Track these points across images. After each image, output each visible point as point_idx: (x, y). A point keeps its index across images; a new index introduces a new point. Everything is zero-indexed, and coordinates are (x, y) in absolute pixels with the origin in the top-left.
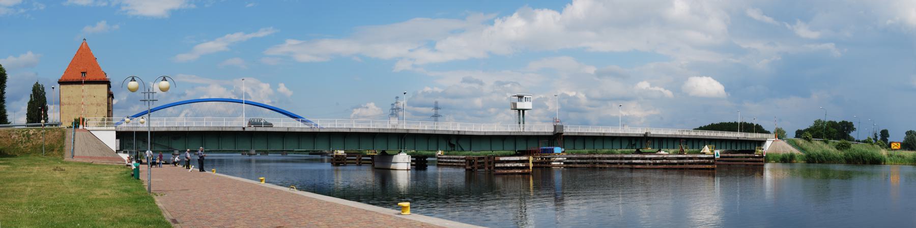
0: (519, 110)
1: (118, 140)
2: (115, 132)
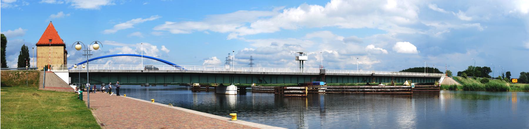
0: (300, 61)
1: (70, 78)
2: (68, 73)
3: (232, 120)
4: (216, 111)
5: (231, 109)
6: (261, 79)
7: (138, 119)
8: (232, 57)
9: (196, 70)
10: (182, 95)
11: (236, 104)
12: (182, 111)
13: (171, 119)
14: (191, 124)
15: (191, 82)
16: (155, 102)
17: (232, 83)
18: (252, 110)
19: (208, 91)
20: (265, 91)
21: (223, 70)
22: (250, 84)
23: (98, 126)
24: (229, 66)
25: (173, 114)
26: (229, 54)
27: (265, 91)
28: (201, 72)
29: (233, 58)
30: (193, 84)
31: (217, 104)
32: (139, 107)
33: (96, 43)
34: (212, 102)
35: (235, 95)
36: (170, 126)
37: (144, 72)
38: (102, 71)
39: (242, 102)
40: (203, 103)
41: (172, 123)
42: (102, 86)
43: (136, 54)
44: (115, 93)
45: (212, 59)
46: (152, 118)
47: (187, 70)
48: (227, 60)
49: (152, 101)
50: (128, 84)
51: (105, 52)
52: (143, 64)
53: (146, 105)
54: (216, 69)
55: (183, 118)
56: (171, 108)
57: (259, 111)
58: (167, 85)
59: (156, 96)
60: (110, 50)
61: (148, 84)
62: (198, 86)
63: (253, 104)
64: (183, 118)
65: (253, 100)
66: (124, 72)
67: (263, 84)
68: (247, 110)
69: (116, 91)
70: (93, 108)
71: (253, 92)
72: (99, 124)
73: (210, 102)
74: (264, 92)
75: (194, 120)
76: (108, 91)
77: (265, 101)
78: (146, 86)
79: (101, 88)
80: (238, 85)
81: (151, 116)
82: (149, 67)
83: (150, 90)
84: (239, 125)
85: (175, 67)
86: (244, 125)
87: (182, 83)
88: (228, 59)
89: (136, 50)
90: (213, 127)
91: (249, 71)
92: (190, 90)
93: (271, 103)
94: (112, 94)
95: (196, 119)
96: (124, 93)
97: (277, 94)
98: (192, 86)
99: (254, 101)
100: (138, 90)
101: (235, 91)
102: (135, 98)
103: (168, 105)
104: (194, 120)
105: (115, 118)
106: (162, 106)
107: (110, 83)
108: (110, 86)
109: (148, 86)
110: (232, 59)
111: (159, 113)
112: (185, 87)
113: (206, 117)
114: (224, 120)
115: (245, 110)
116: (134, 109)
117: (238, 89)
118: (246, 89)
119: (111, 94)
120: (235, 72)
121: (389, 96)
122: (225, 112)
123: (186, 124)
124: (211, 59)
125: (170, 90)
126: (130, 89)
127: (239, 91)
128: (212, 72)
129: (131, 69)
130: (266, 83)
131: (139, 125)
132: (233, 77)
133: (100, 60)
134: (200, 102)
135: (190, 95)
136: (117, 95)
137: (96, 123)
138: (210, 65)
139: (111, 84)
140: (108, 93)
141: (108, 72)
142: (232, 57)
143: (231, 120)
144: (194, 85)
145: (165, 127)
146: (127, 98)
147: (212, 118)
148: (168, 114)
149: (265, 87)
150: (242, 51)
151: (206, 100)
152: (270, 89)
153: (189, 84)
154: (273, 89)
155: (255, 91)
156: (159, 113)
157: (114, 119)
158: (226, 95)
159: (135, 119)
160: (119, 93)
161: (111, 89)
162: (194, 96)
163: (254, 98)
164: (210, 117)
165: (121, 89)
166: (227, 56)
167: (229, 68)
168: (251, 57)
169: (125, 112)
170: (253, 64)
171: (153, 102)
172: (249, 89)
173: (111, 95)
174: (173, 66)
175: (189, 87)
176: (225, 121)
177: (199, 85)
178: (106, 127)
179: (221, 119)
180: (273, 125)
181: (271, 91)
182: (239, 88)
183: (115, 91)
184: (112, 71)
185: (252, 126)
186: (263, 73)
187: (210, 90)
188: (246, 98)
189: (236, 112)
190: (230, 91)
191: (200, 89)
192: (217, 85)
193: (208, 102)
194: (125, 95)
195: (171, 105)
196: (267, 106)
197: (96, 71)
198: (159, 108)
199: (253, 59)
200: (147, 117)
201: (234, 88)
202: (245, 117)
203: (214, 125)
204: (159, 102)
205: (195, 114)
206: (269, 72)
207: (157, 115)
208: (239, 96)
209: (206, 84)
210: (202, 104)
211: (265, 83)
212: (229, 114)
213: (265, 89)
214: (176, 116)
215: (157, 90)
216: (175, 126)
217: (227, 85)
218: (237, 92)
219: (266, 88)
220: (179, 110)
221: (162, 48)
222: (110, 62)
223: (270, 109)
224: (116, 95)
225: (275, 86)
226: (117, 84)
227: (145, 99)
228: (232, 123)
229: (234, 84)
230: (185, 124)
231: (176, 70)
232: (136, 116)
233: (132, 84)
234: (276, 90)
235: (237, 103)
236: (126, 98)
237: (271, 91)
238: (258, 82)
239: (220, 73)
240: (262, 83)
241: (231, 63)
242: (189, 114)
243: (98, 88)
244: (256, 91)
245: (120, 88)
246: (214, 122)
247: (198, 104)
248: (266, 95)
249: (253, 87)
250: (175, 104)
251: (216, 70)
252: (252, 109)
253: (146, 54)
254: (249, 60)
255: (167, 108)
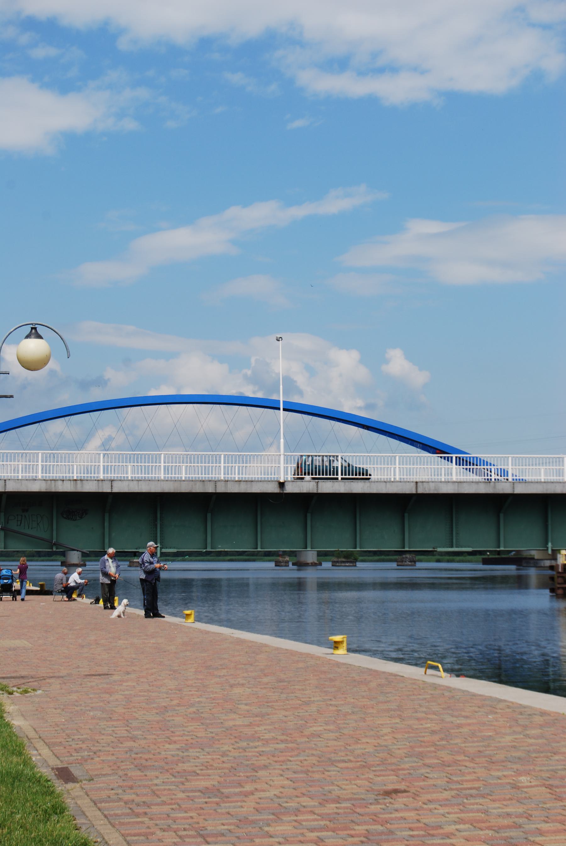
7: (260, 743)
10: (499, 614)
12: (266, 646)
13: (434, 745)
14: (555, 771)
15: (547, 543)
16: (349, 650)
23: (38, 780)
25: (449, 719)
32: (265, 680)
33: (34, 333)
36: (431, 782)
37: (290, 489)
38: (68, 488)
41: (444, 764)
42: (65, 569)
43: (249, 392)
44: (140, 603)
46: (332, 735)
49: (336, 645)
50: (208, 553)
51: (84, 385)
52: (287, 447)
53: (301, 665)
55: (509, 738)
56: (435, 687)
58: (414, 562)
59: (359, 619)
60: (109, 374)
61: (311, 556)
64: (509, 738)
66: (184, 488)
69: (140, 591)
70: (15, 682)
72: (45, 772)
76: (100, 592)
78: (301, 565)
79: (59, 575)
81: (332, 727)
82: (318, 462)
83: (323, 586)
85: (460, 461)
87: (499, 553)
89: (249, 372)
92: (542, 586)
94: (120, 609)
96: (187, 602)
98: (552, 568)
100: (259, 586)
102: (241, 628)
103: (421, 670)
105: (134, 739)
106: (391, 674)
107: (111, 550)
108: (112, 568)
109: (314, 564)
111: (371, 711)
112: (511, 569)
116: (237, 690)
119: (113, 608)
123: (528, 773)
125: (433, 585)
126: (219, 580)
129: (222, 477)
131: (261, 773)
133: (57, 425)
135: (541, 612)
136: (147, 616)
137: (26, 762)
139: (112, 556)
140: (97, 601)
141: (100, 491)
145: (402, 787)
146: (201, 631)
148: (420, 715)
156: (371, 711)
157: (130, 744)
159: (244, 744)
160: (159, 604)
161: (113, 582)
165: (169, 583)
169: (192, 705)
171: (342, 651)
173: (116, 613)
174: (450, 460)
175: (532, 572)
178: (88, 786)
183: (138, 593)
184: (118, 488)
185: (274, 645)
194: (188, 616)
195: (436, 668)
197: (35, 487)
198: (373, 685)
200: (307, 732)
204: (373, 653)
207: (364, 720)
214: (465, 730)
215: (360, 586)
216: (458, 782)
220: (483, 698)
221: (387, 361)
222: (110, 439)
224: (143, 613)
226: (147, 557)
227: (296, 637)
230: (519, 773)
231: (462, 478)
232: (250, 725)
233: (226, 553)
236: (195, 629)
242: (538, 719)
243: (42, 576)
245: (163, 575)
250: (457, 662)
253: (301, 393)
255: (414, 682)
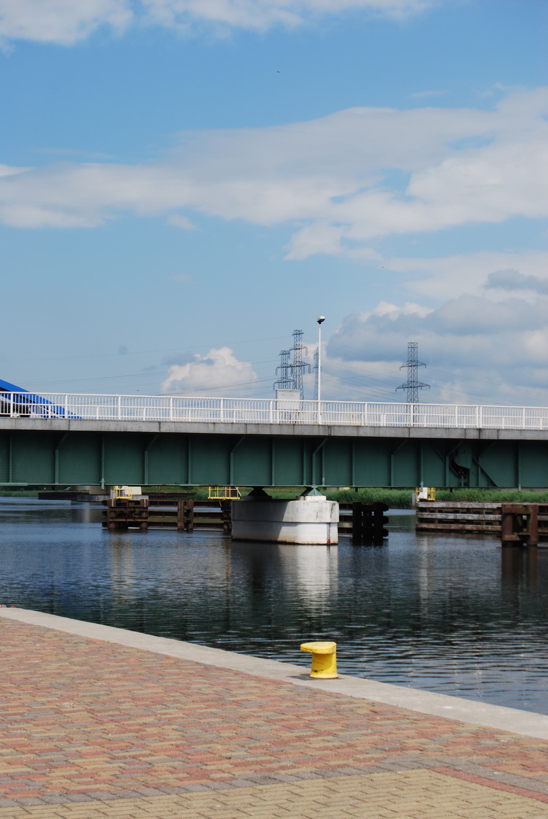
3: (314, 675)
4: (228, 627)
5: (310, 619)
6: (465, 461)
8: (312, 349)
9: (127, 417)
10: (52, 545)
11: (332, 595)
14: (97, 696)
17: (314, 486)
18: (418, 628)
19: (187, 524)
20: (453, 526)
21: (266, 415)
22: (406, 492)
24: (297, 395)
26: (298, 333)
27: (453, 526)
28: (154, 429)
29: (317, 354)
30: (108, 488)
31: (234, 592)
34: (210, 584)
35: (329, 544)
39: (364, 581)
40: (161, 590)
45: (210, 362)
47: (80, 419)
48: (285, 367)
54: (231, 414)
57: (452, 631)
62: (137, 502)
63: (424, 595)
65: (424, 573)
67: (475, 491)
68: (389, 625)
71: (420, 532)
73: (198, 582)
74: (447, 532)
75: (118, 679)
77: (451, 575)
80: (345, 495)
84: (351, 701)
86: (373, 704)
87: (54, 487)
88: (290, 362)
90: (215, 715)
91: (402, 424)
92: (94, 520)
93: (483, 588)
95: (125, 673)
97: (514, 544)
98: (105, 503)
99: (429, 578)
101: (325, 526)
104: (118, 679)
110: (312, 362)
112: (66, 504)
113: (177, 663)
114: (272, 677)
115: (381, 624)
117: (343, 518)
118: (385, 513)
120: (329, 427)
121: (453, 534)
122: (275, 634)
123: (71, 699)
124: (203, 362)
127: (347, 525)
128: (210, 430)
130: (492, 485)
132: (320, 454)
134: (144, 583)
135: (93, 545)
138: (200, 389)
142: (312, 349)
143: (305, 677)
144: (114, 496)
147: (207, 668)
149: (451, 505)
150: (364, 317)
151: (179, 573)
152: (475, 517)
153: (88, 488)
154: (491, 517)
155: (432, 526)
158: (283, 549)
162: (112, 551)
163: (425, 563)
164: (198, 663)
166: (288, 344)
167: (297, 406)
168: (413, 347)
170: (422, 385)
172: (403, 519)
175: (86, 508)
176: (278, 684)
177: (143, 494)
179: (255, 673)
180: (526, 704)
181: (484, 527)
182: (349, 513)
185: (415, 709)
186: (473, 435)
187: (196, 520)
188: (387, 561)
189: (336, 633)
190: (300, 526)
191: (144, 515)
192: (234, 493)
193: (190, 582)
196: (459, 602)
199: (421, 359)
201: (321, 511)
202: (379, 664)
203: (220, 701)
205: (121, 646)
206: (503, 426)
208: (348, 550)
209: (179, 491)
210: (155, 595)
211: (483, 482)
212: (297, 646)
213: (451, 516)
214: (13, 658)
217: (288, 495)
218: (341, 530)
219: (456, 511)
223: (477, 618)
225: (505, 500)
228: (315, 693)
229: (322, 490)
230: (63, 699)
234: (509, 519)
235: (340, 586)
237: (484, 527)
238: (451, 480)
239: (252, 431)
240: (467, 485)
241: (307, 378)
242: (83, 647)
244: (440, 526)
246: (215, 689)
247: (137, 593)
248: (458, 547)
249: (422, 505)
251: (229, 420)
252: (418, 618)
254: (400, 364)
